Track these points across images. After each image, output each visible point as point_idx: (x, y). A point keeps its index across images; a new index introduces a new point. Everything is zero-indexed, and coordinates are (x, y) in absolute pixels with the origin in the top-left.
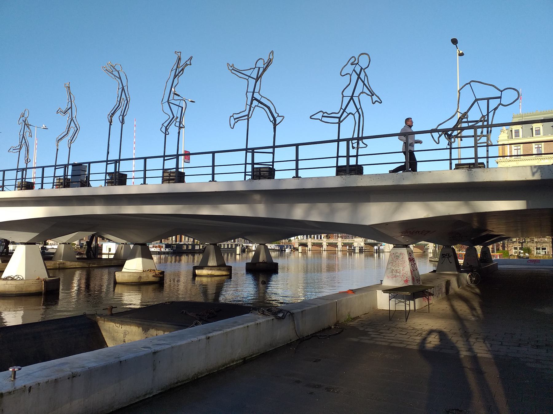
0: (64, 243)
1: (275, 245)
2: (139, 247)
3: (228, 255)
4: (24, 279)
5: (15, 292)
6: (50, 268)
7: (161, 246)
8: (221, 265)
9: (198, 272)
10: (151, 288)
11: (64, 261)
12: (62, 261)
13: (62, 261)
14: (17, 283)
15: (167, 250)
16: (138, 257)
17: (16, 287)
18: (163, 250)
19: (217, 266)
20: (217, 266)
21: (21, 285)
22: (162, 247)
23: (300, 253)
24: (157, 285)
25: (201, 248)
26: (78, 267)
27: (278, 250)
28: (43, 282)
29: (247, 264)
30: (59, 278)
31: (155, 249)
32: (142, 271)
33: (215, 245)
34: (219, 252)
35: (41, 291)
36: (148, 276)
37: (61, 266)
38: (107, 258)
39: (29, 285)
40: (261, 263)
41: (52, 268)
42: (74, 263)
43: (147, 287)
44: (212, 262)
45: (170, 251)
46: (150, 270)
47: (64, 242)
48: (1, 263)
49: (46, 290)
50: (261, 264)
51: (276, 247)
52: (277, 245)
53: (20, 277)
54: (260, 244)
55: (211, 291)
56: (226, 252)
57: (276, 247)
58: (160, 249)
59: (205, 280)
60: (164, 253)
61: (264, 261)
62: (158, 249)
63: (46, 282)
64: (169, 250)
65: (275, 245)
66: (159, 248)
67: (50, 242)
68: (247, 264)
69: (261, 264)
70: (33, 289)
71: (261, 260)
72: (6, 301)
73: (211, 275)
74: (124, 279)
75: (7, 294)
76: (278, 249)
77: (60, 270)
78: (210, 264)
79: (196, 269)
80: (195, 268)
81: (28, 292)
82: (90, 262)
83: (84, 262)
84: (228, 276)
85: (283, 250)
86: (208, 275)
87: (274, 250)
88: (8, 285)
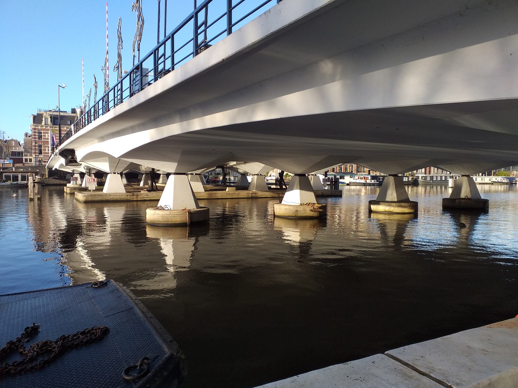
0: (257, 175)
1: (503, 178)
2: (298, 178)
3: (441, 188)
4: (172, 209)
5: (161, 221)
6: (204, 198)
7: (366, 177)
8: (403, 200)
9: (373, 207)
10: (309, 223)
11: (256, 191)
12: (255, 191)
13: (255, 191)
14: (163, 213)
15: (373, 181)
16: (296, 189)
17: (162, 217)
18: (368, 181)
19: (398, 202)
20: (398, 202)
21: (167, 215)
22: (367, 179)
23: (450, 187)
24: (315, 221)
25: (410, 180)
26: (268, 196)
27: (507, 184)
28: (187, 213)
29: (444, 200)
30: (209, 209)
31: (361, 180)
32: (300, 205)
33: (395, 176)
34: (400, 185)
35: (185, 222)
36: (305, 210)
37: (253, 195)
38: (275, 187)
39: (174, 215)
40: (463, 199)
41: (206, 198)
42: (265, 192)
43: (305, 222)
44: (392, 195)
45: (376, 182)
46: (308, 204)
47: (257, 174)
48: (204, 191)
49: (191, 221)
50: (463, 201)
51: (503, 179)
52: (505, 178)
53: (167, 206)
54: (296, 175)
55: (392, 231)
56: (438, 185)
57: (503, 179)
58: (365, 180)
59: (381, 217)
60: (370, 185)
61: (467, 197)
62: (364, 180)
63: (191, 213)
64: (375, 181)
65: (503, 178)
66: (365, 179)
67: (212, 172)
68: (444, 200)
69: (463, 201)
70: (178, 219)
71: (463, 195)
72: (153, 228)
73: (389, 212)
74: (281, 213)
75: (156, 224)
76: (506, 181)
77: (253, 199)
78: (388, 199)
79: (372, 204)
80: (371, 203)
81: (174, 223)
82: (280, 192)
83: (273, 192)
84: (412, 215)
85: (514, 183)
86: (386, 211)
87: (500, 183)
88: (156, 215)
